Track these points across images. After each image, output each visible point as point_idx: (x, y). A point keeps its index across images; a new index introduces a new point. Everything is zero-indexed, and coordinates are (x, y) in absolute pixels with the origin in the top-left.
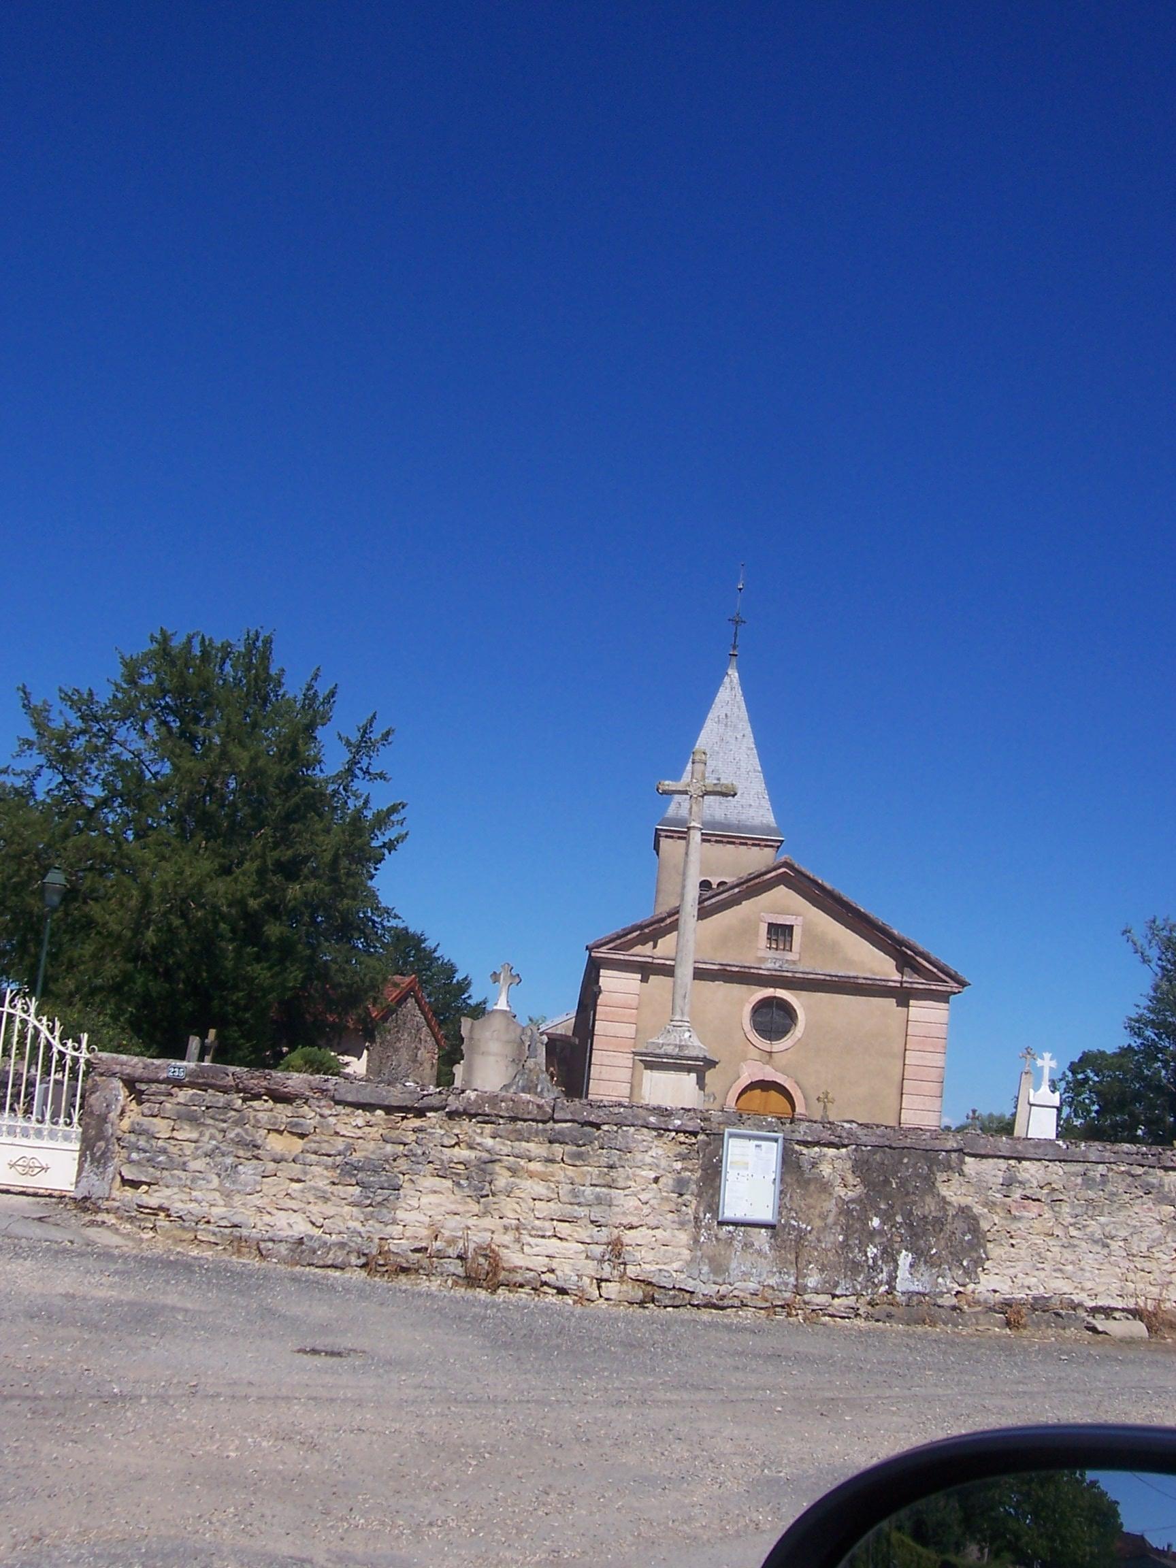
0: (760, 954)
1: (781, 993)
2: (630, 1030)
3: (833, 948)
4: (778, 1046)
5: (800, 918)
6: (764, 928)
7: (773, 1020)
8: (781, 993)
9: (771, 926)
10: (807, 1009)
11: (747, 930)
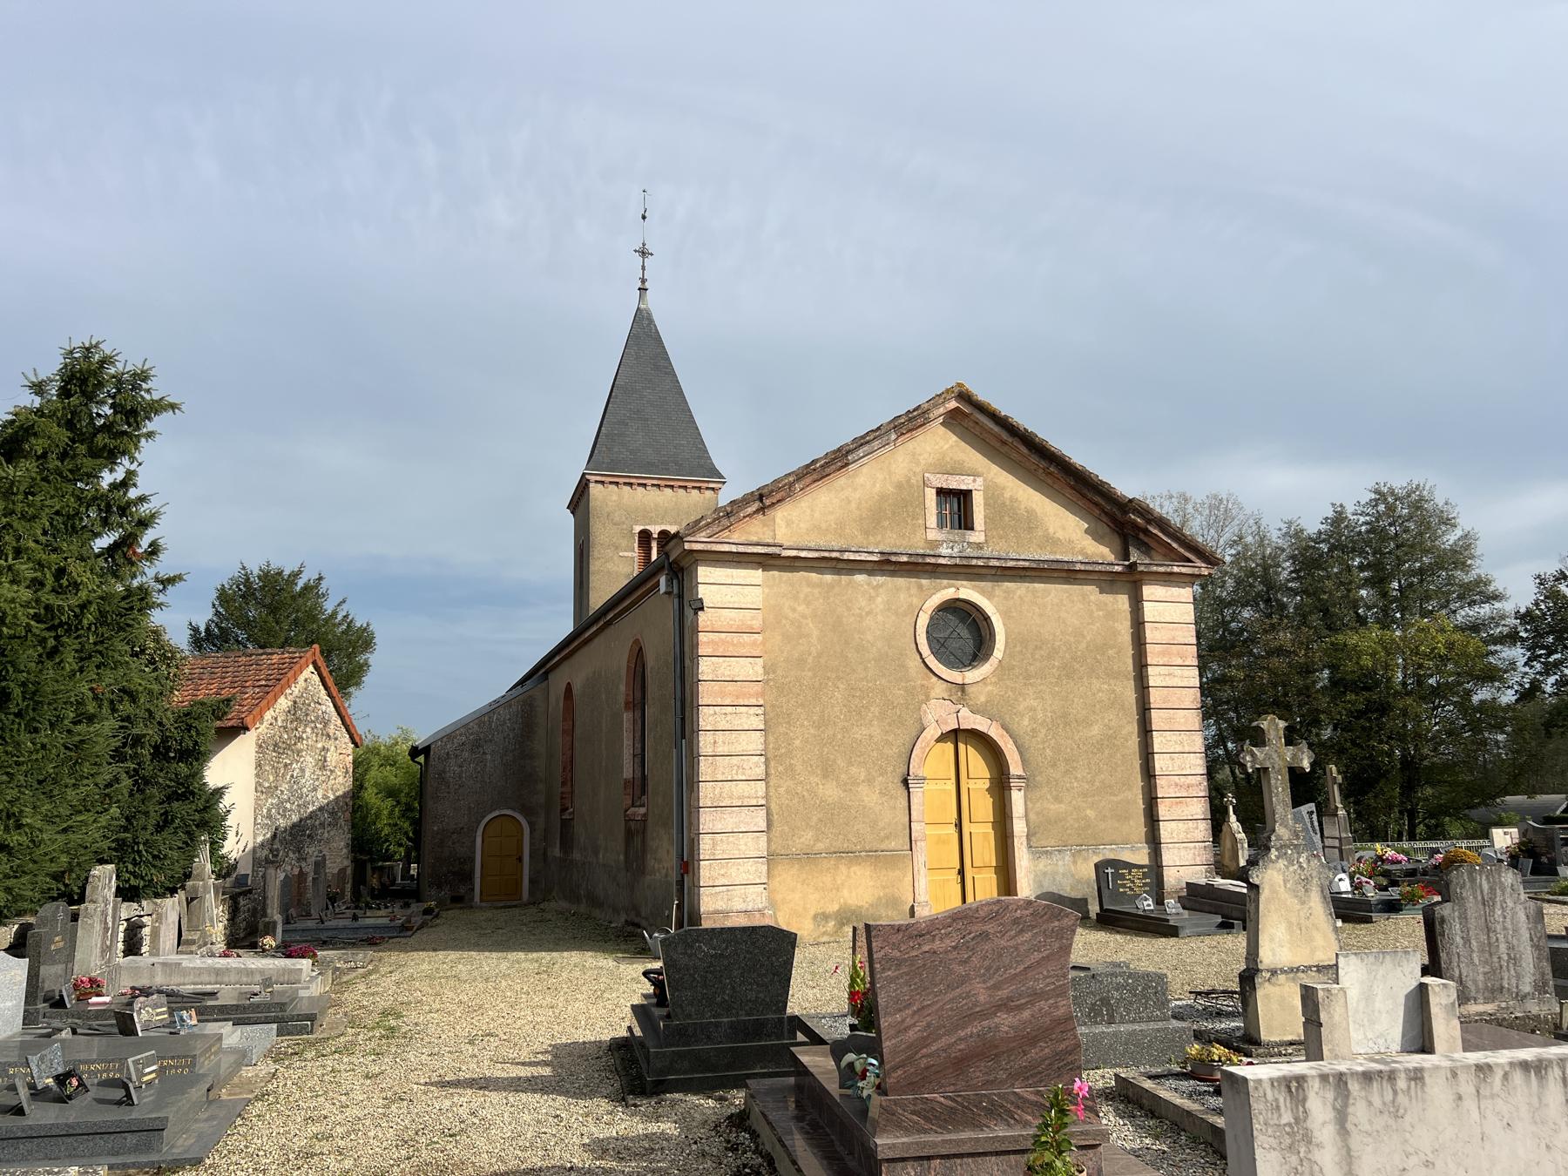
0: (928, 532)
1: (967, 591)
2: (753, 669)
3: (1030, 522)
4: (971, 676)
5: (980, 480)
6: (931, 494)
7: (963, 634)
8: (967, 591)
9: (941, 492)
10: (1006, 615)
11: (902, 504)
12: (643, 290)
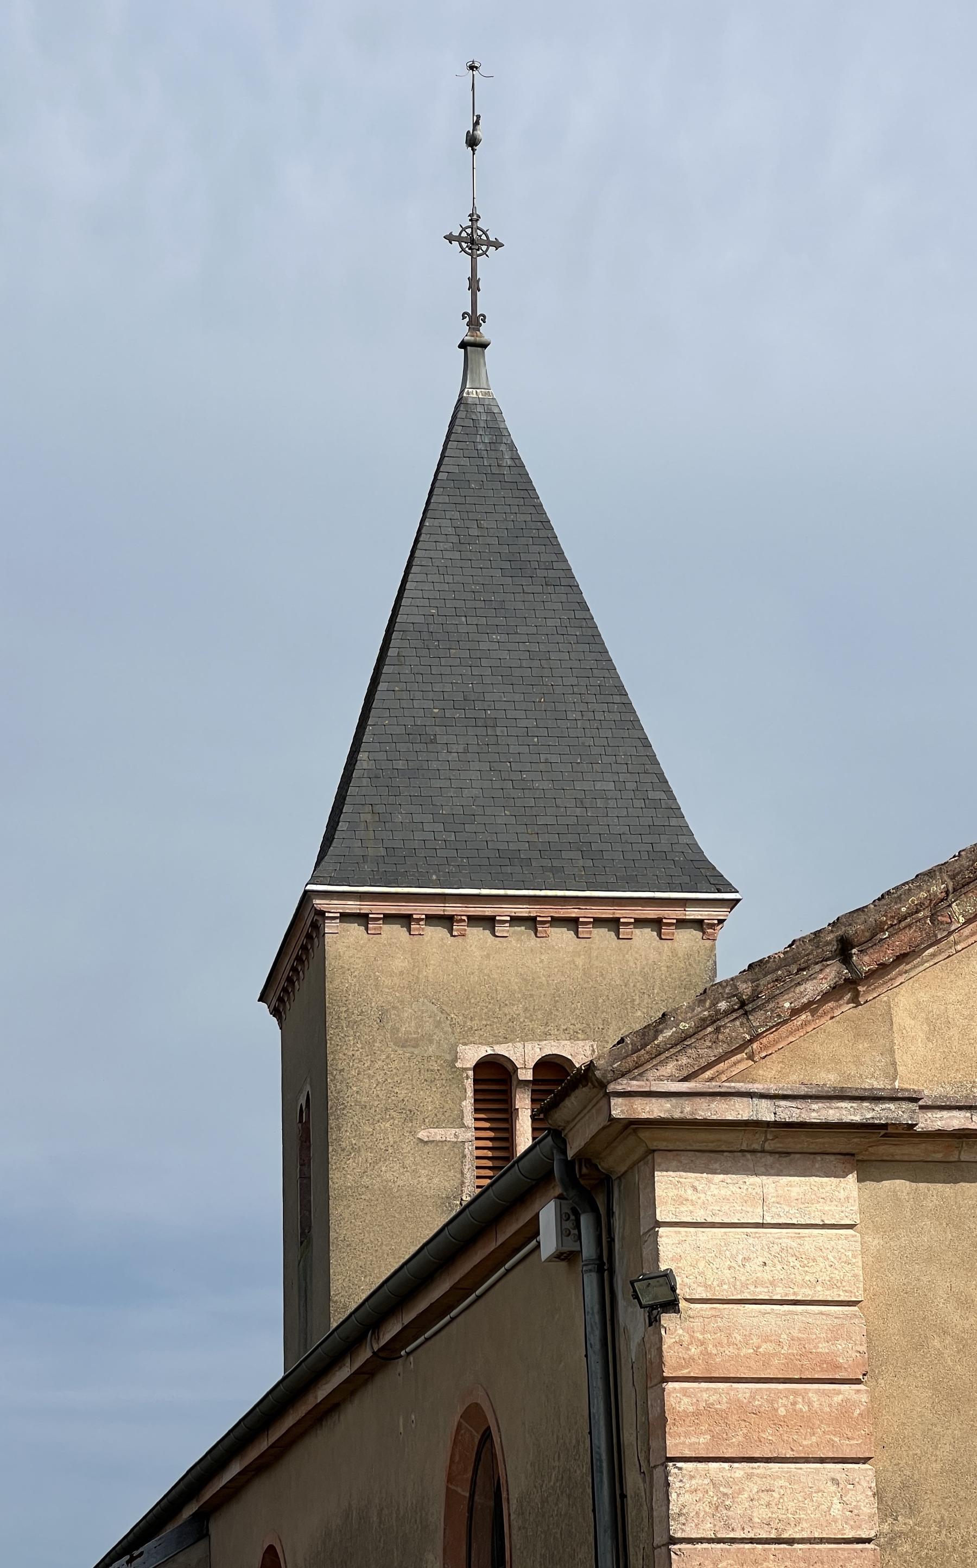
12: (473, 347)
